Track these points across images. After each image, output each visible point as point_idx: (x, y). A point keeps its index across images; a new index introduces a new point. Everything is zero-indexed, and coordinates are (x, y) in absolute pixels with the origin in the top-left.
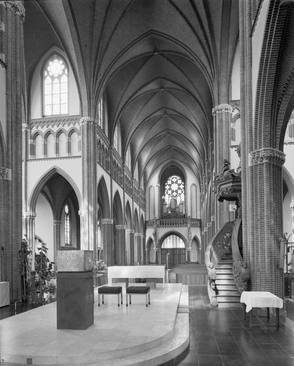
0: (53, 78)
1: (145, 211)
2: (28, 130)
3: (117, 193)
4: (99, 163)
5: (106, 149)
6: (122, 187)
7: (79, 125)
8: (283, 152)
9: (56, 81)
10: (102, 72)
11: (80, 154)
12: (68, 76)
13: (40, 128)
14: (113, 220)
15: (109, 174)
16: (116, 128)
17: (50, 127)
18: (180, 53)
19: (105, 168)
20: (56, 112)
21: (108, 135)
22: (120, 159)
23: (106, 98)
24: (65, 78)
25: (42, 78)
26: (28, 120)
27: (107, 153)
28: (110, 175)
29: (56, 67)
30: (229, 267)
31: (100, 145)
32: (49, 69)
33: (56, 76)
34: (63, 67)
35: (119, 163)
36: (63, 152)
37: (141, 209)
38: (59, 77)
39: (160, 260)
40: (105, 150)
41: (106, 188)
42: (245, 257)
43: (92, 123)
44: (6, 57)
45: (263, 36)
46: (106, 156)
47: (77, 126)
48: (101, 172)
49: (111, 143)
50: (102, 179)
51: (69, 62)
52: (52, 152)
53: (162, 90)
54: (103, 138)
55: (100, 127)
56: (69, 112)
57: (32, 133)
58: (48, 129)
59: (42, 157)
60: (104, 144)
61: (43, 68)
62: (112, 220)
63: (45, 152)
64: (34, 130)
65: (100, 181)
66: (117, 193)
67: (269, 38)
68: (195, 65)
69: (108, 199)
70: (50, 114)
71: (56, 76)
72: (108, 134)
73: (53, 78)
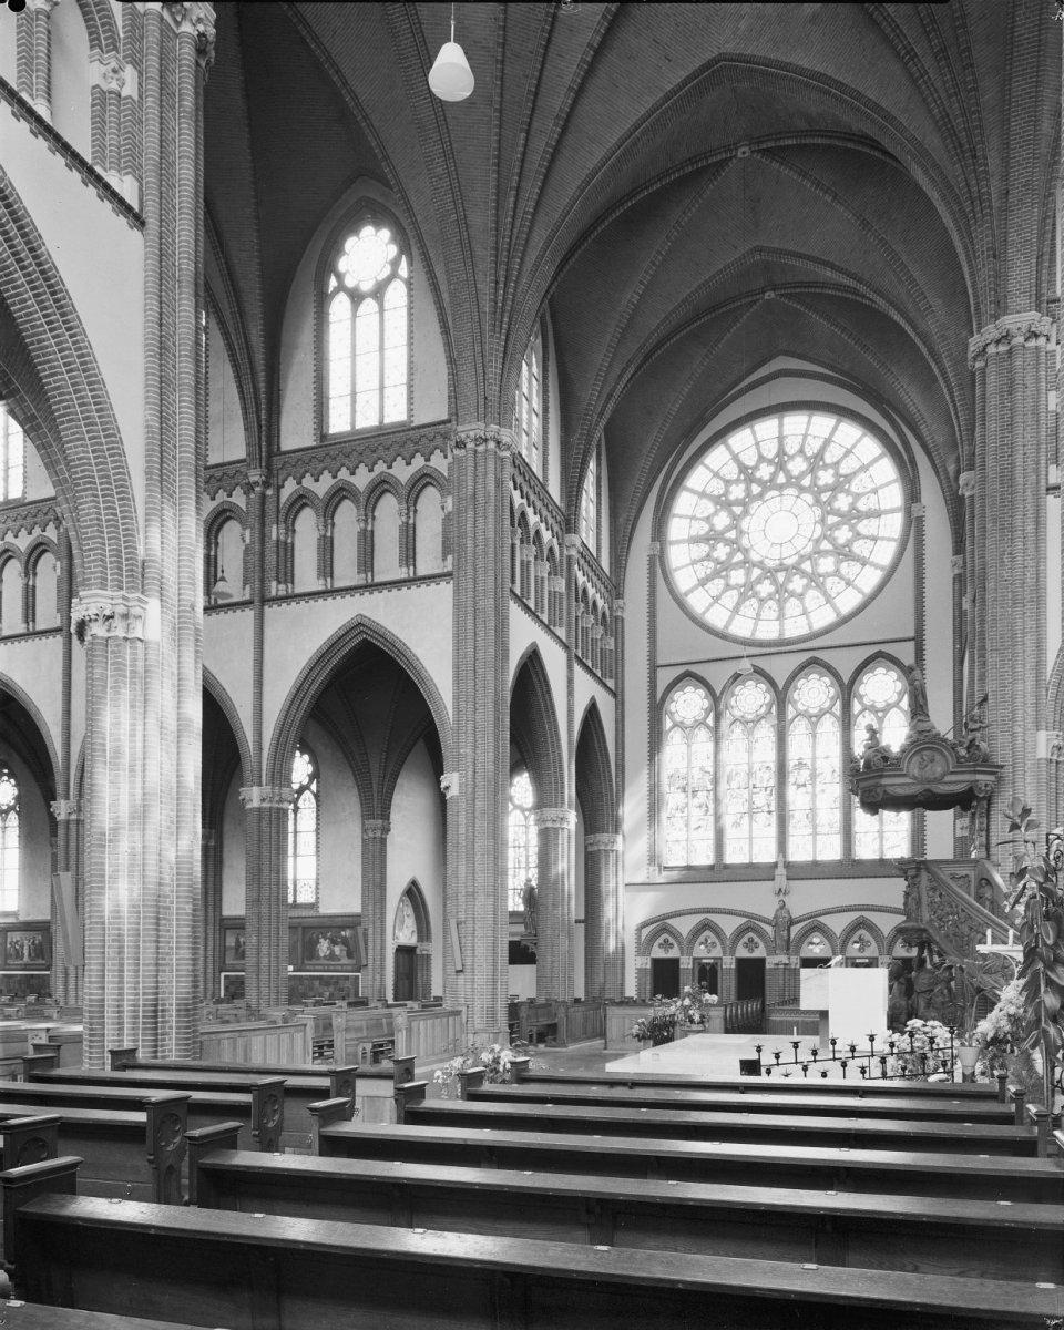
0: (356, 297)
1: (617, 695)
2: (269, 492)
4: (521, 601)
7: (446, 457)
9: (369, 305)
12: (409, 283)
13: (308, 482)
17: (344, 474)
18: (824, 285)
19: (545, 618)
20: (367, 420)
24: (397, 294)
25: (322, 300)
26: (270, 455)
27: (554, 560)
29: (368, 253)
31: (587, 604)
32: (343, 264)
33: (366, 287)
34: (393, 250)
35: (589, 585)
36: (388, 564)
38: (378, 293)
40: (580, 592)
41: (551, 700)
42: (186, 982)
44: (616, 684)
46: (549, 574)
48: (524, 633)
50: (532, 660)
51: (409, 240)
52: (346, 570)
56: (410, 410)
57: (283, 499)
58: (336, 480)
59: (318, 586)
60: (543, 526)
61: (327, 265)
63: (326, 568)
64: (290, 488)
68: (876, 311)
70: (347, 428)
71: (366, 287)
72: (611, 563)
73: (356, 297)
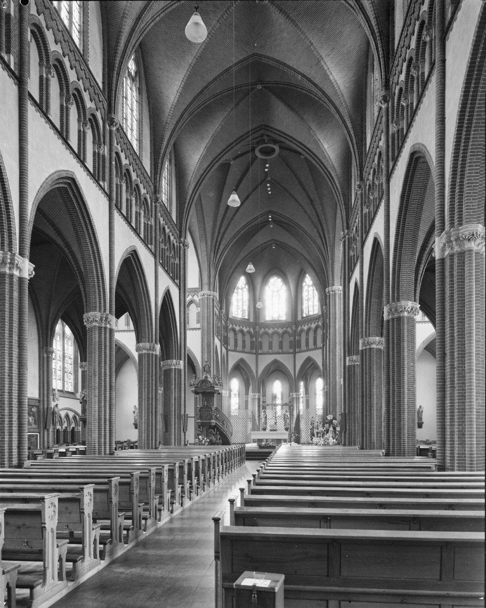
3: (168, 294)
5: (145, 199)
6: (102, 189)
8: (435, 339)
10: (222, 247)
11: (198, 326)
14: (159, 346)
15: (151, 251)
16: (167, 164)
19: (142, 236)
21: (103, 83)
22: (148, 179)
23: (173, 161)
28: (155, 255)
30: (97, 332)
37: (119, 222)
39: (347, 443)
43: (211, 297)
45: (467, 61)
47: (196, 298)
49: (110, 105)
53: (259, 87)
54: (169, 224)
55: (81, 58)
60: (171, 234)
62: (158, 347)
65: (164, 297)
66: (168, 294)
67: (478, 71)
69: (149, 302)
72: (177, 216)
